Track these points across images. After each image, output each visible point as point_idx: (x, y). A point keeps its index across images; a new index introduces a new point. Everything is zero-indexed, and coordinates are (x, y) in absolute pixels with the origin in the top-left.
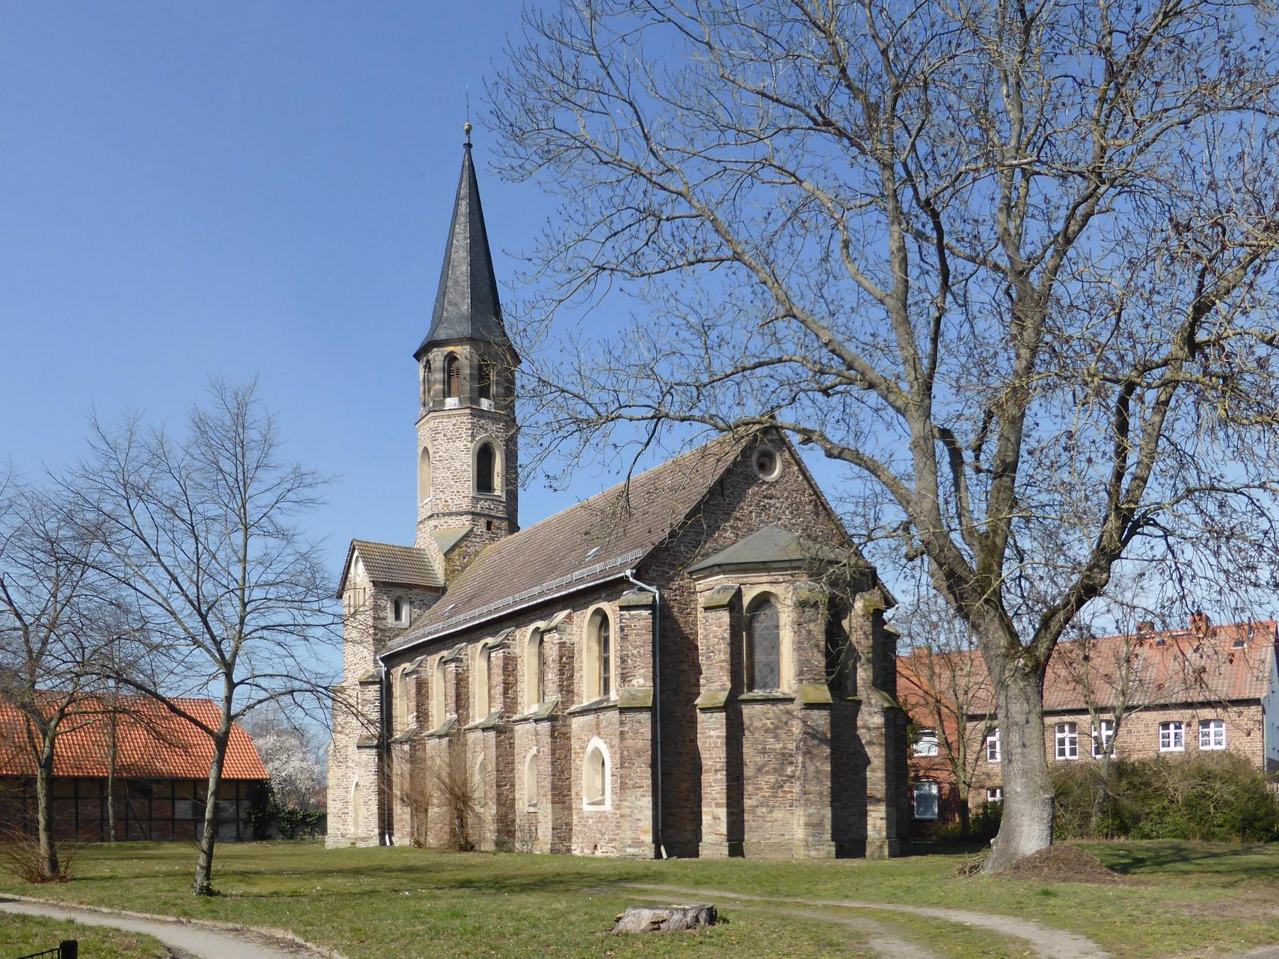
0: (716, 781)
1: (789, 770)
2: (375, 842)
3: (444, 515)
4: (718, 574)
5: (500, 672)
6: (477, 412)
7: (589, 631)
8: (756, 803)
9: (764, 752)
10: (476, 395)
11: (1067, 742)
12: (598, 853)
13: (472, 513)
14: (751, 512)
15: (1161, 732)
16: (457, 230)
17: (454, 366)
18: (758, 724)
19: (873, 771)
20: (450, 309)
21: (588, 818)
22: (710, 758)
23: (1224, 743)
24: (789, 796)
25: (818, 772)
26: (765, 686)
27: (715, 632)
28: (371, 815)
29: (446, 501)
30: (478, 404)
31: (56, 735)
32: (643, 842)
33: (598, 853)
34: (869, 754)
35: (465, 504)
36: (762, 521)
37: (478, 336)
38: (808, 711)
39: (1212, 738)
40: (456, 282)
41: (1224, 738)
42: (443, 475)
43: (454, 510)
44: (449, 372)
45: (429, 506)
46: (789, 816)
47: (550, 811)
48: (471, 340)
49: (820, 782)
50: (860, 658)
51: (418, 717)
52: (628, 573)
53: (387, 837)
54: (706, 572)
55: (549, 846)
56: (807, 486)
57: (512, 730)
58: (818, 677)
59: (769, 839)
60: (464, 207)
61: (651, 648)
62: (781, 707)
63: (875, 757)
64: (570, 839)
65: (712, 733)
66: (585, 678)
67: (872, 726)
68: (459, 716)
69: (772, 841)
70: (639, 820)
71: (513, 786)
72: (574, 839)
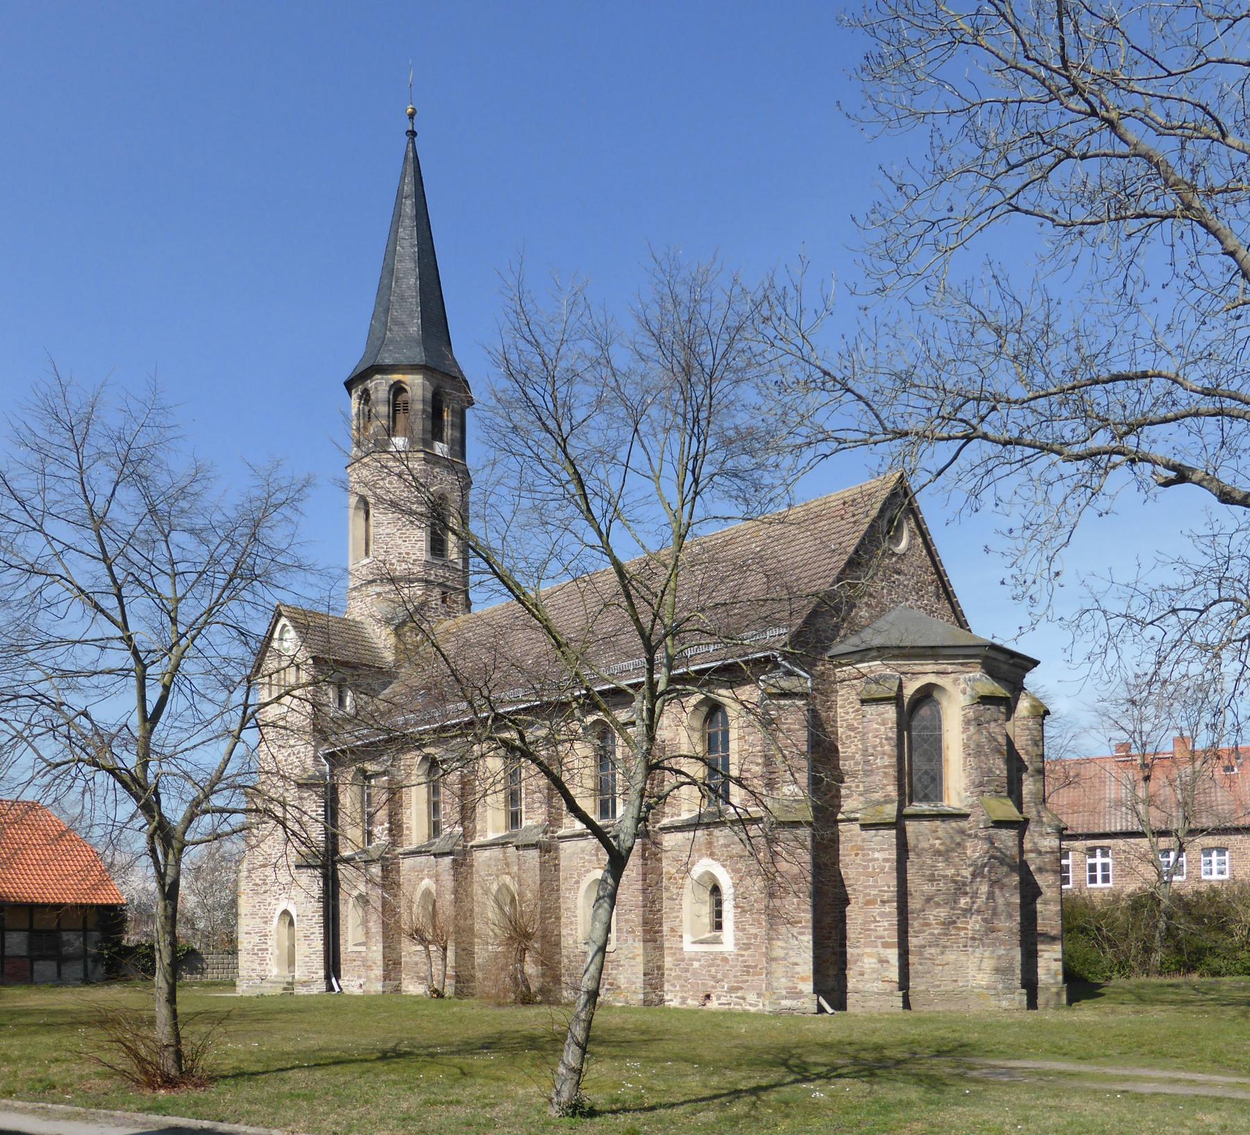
0: (882, 915)
1: (963, 902)
2: (320, 987)
4: (874, 659)
6: (431, 457)
8: (923, 942)
9: (932, 879)
10: (429, 436)
11: (1099, 868)
12: (713, 1005)
14: (883, 589)
15: (1203, 858)
17: (400, 399)
18: (925, 845)
19: (1046, 903)
20: (395, 328)
21: (691, 960)
22: (875, 887)
23: (1227, 872)
24: (962, 933)
25: (1008, 904)
26: (926, 798)
27: (877, 730)
28: (315, 953)
31: (184, 845)
32: (801, 992)
33: (713, 1005)
34: (1040, 883)
36: (893, 601)
37: (432, 364)
38: (997, 830)
39: (1215, 867)
40: (402, 298)
41: (1227, 867)
42: (388, 531)
44: (395, 405)
46: (963, 958)
47: (641, 951)
48: (423, 369)
49: (1010, 916)
50: (1027, 768)
51: (390, 830)
53: (334, 980)
54: (857, 657)
55: (641, 996)
56: (929, 563)
57: (557, 849)
58: (999, 789)
59: (939, 986)
60: (409, 207)
62: (954, 824)
63: (1048, 886)
64: (662, 986)
65: (877, 855)
67: (1043, 850)
68: (464, 829)
69: (942, 988)
70: (797, 964)
71: (558, 918)
72: (666, 987)
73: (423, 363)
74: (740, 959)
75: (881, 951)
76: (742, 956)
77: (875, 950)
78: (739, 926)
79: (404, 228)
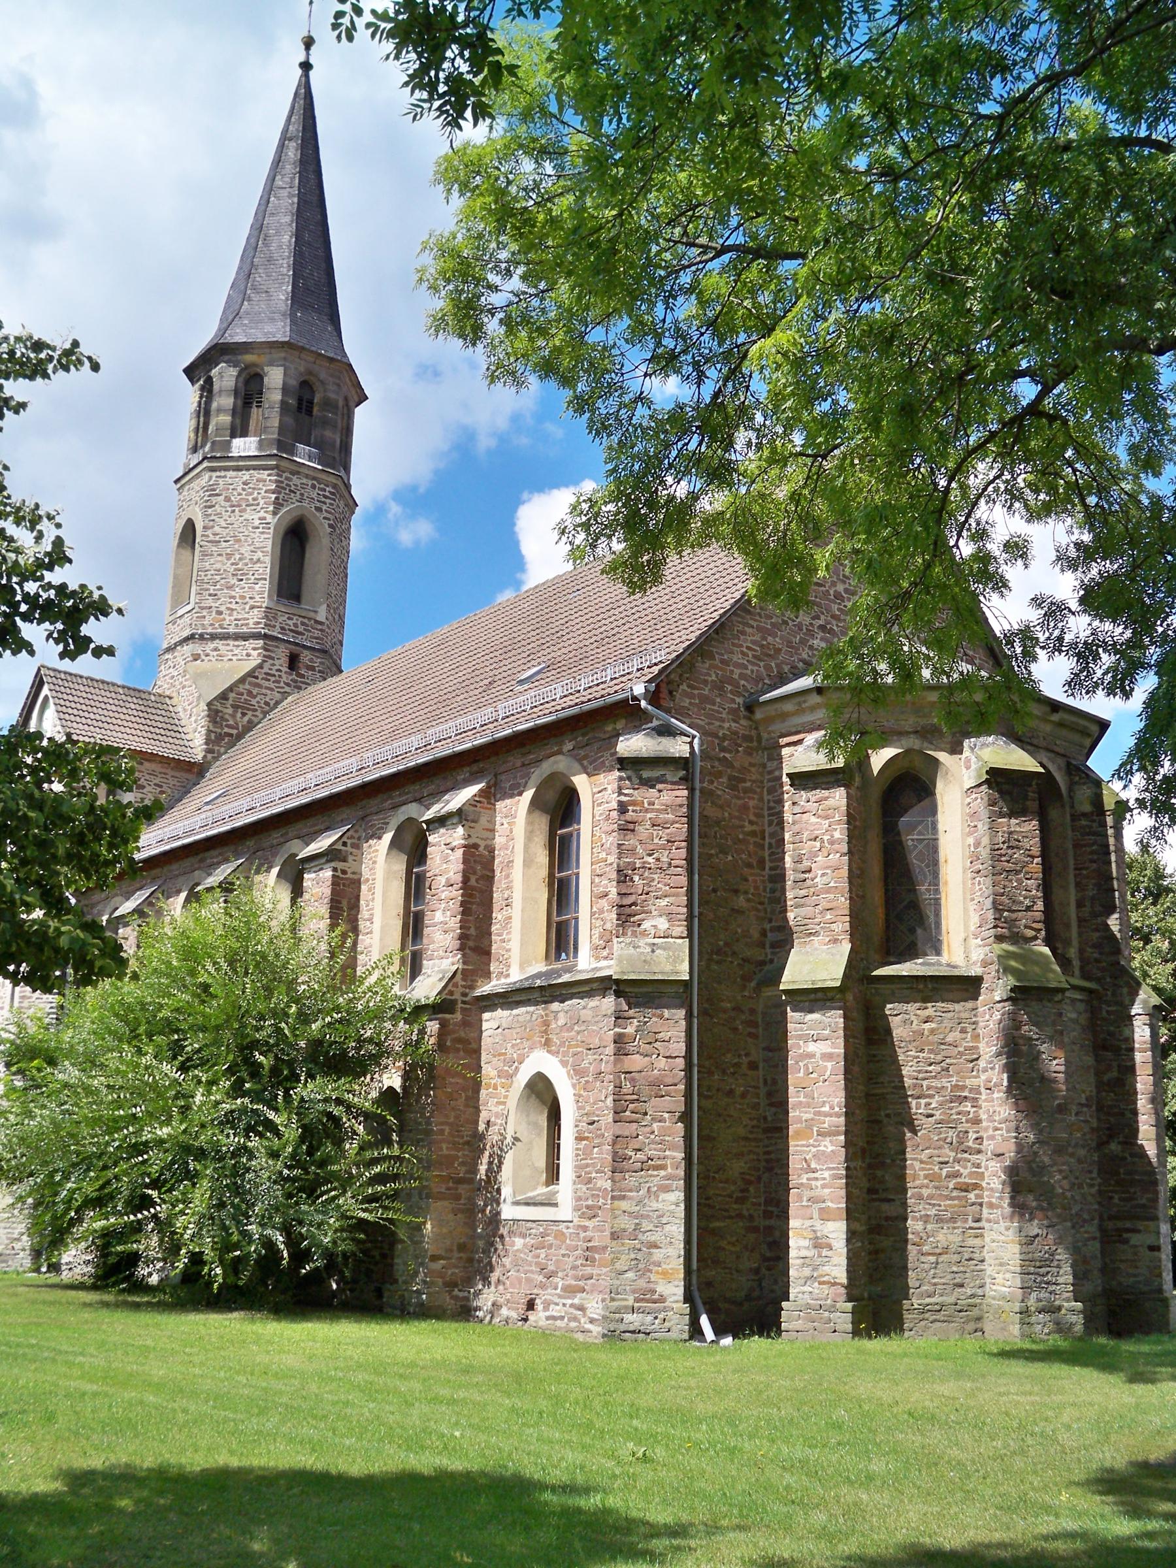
3: (213, 637)
5: (324, 910)
7: (529, 823)
13: (266, 637)
16: (279, 182)
22: (808, 1105)
29: (220, 613)
30: (292, 451)
35: (253, 620)
37: (302, 342)
43: (232, 630)
45: (186, 620)
52: (639, 689)
61: (683, 853)
65: (812, 1047)
66: (516, 924)
73: (287, 339)
74: (582, 1235)
75: (818, 1225)
76: (585, 1229)
77: (808, 1223)
78: (582, 1178)
79: (283, 176)
